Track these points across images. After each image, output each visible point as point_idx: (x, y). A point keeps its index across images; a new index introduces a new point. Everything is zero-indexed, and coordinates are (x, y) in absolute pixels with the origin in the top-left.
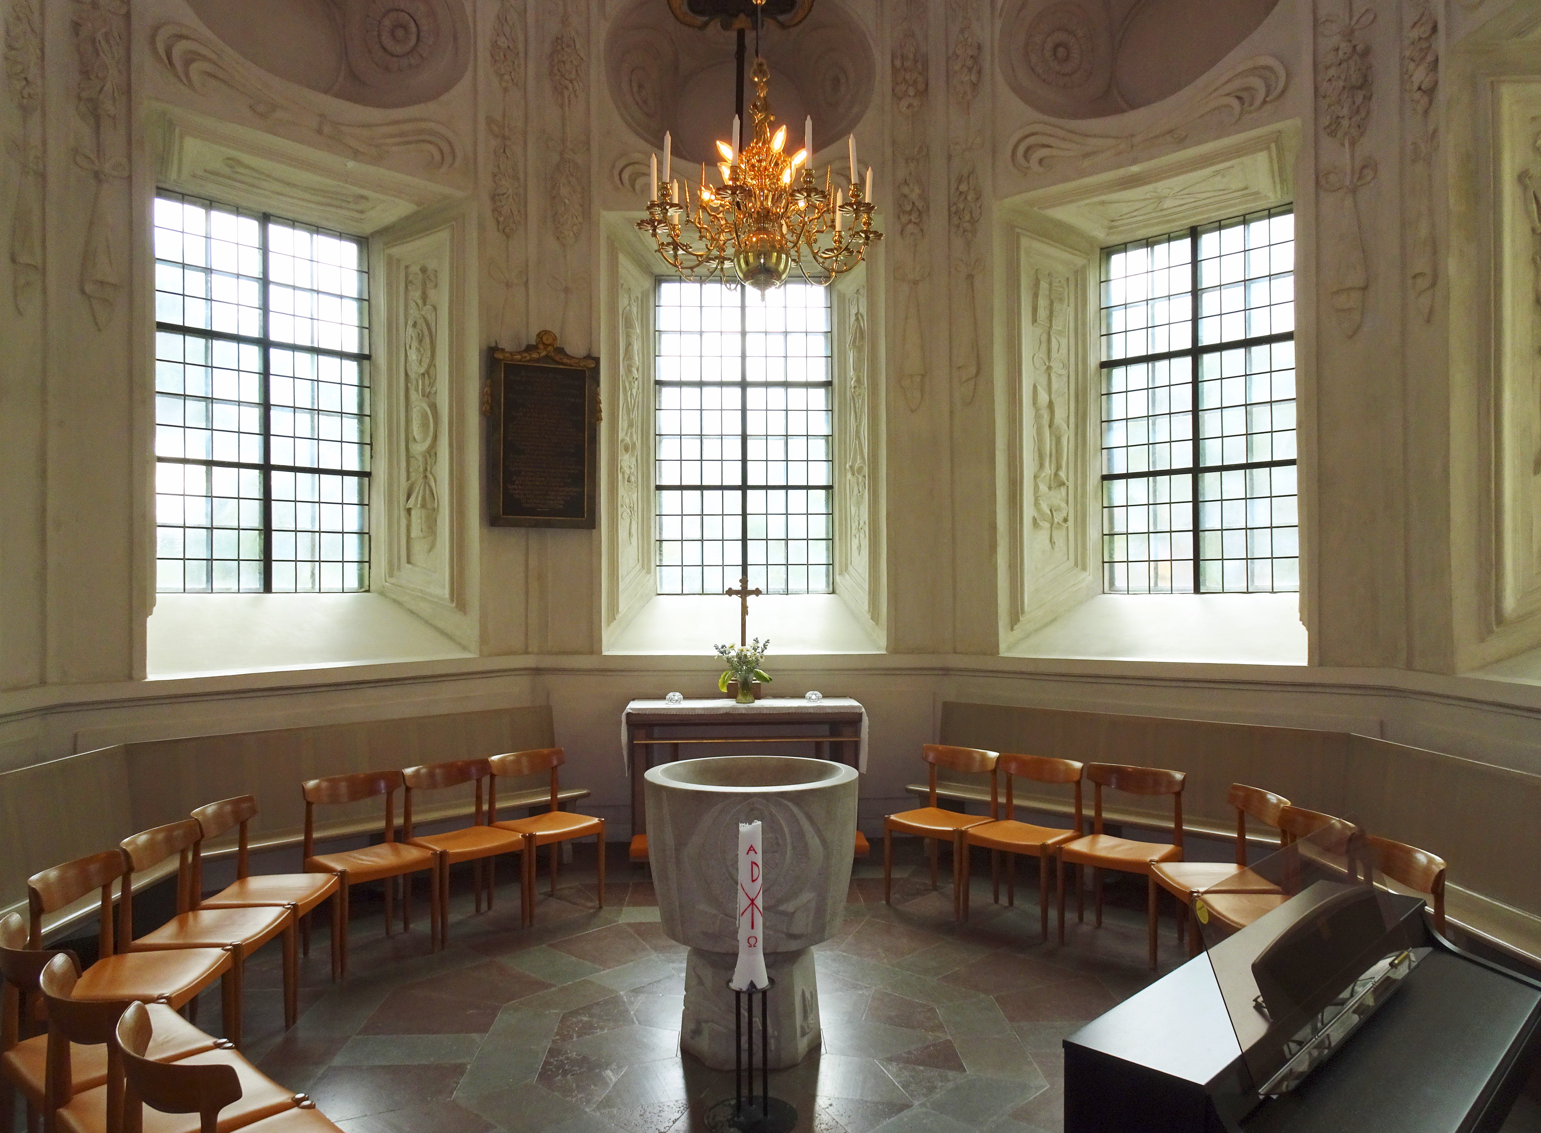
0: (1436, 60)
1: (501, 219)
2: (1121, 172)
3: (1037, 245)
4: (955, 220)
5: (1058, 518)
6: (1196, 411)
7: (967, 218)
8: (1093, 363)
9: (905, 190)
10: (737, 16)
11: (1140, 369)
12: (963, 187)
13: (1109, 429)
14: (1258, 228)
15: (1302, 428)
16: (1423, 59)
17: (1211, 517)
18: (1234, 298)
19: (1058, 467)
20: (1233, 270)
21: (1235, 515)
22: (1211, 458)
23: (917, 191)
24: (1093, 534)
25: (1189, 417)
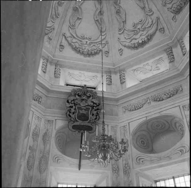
1: (29, 166)
3: (143, 179)
10: (81, 130)
12: (126, 166)
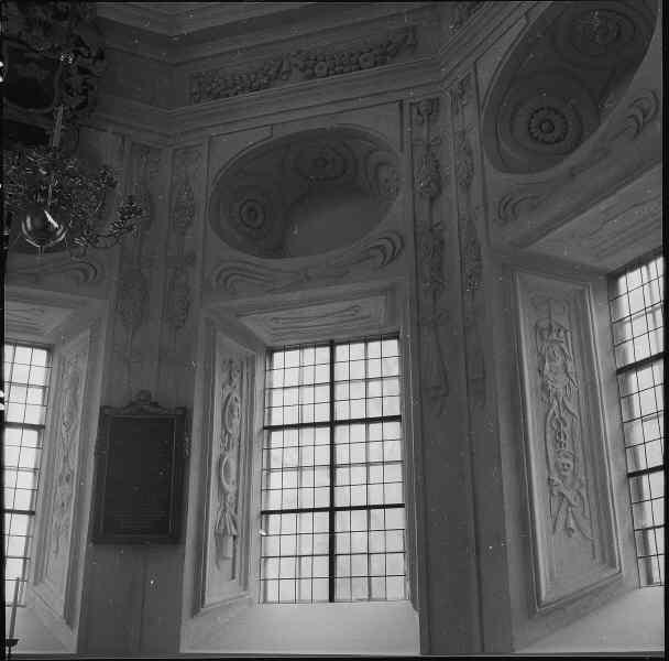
18: (359, 474)
21: (359, 542)
25: (328, 387)
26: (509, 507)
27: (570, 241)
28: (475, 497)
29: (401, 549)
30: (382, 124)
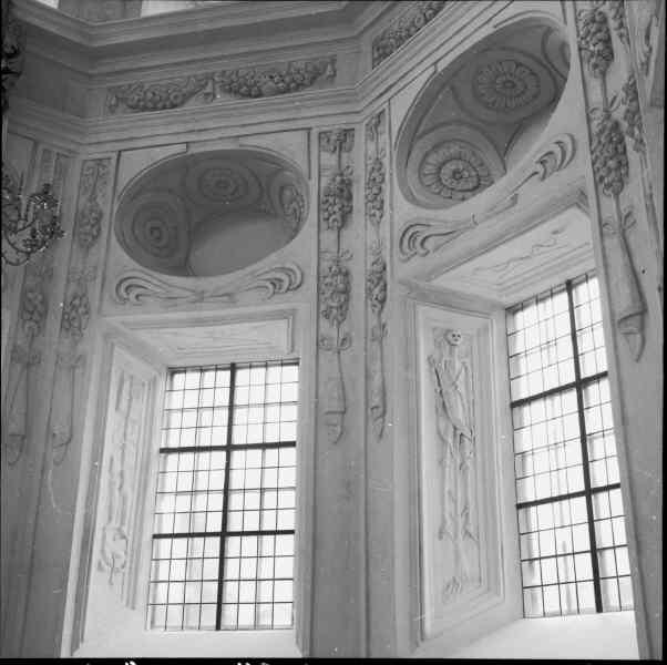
0: (385, 285)
2: (195, 314)
3: (128, 357)
4: (66, 324)
5: (118, 565)
6: (221, 581)
7: (76, 324)
8: (156, 449)
9: (30, 295)
11: (189, 456)
12: (77, 302)
13: (162, 498)
14: (275, 371)
15: (299, 509)
16: (378, 284)
17: (232, 570)
19: (122, 523)
20: (249, 569)
22: (234, 526)
23: (40, 297)
24: (143, 579)
26: (400, 497)
27: (479, 278)
28: (367, 552)
29: (292, 553)
30: (290, 147)
